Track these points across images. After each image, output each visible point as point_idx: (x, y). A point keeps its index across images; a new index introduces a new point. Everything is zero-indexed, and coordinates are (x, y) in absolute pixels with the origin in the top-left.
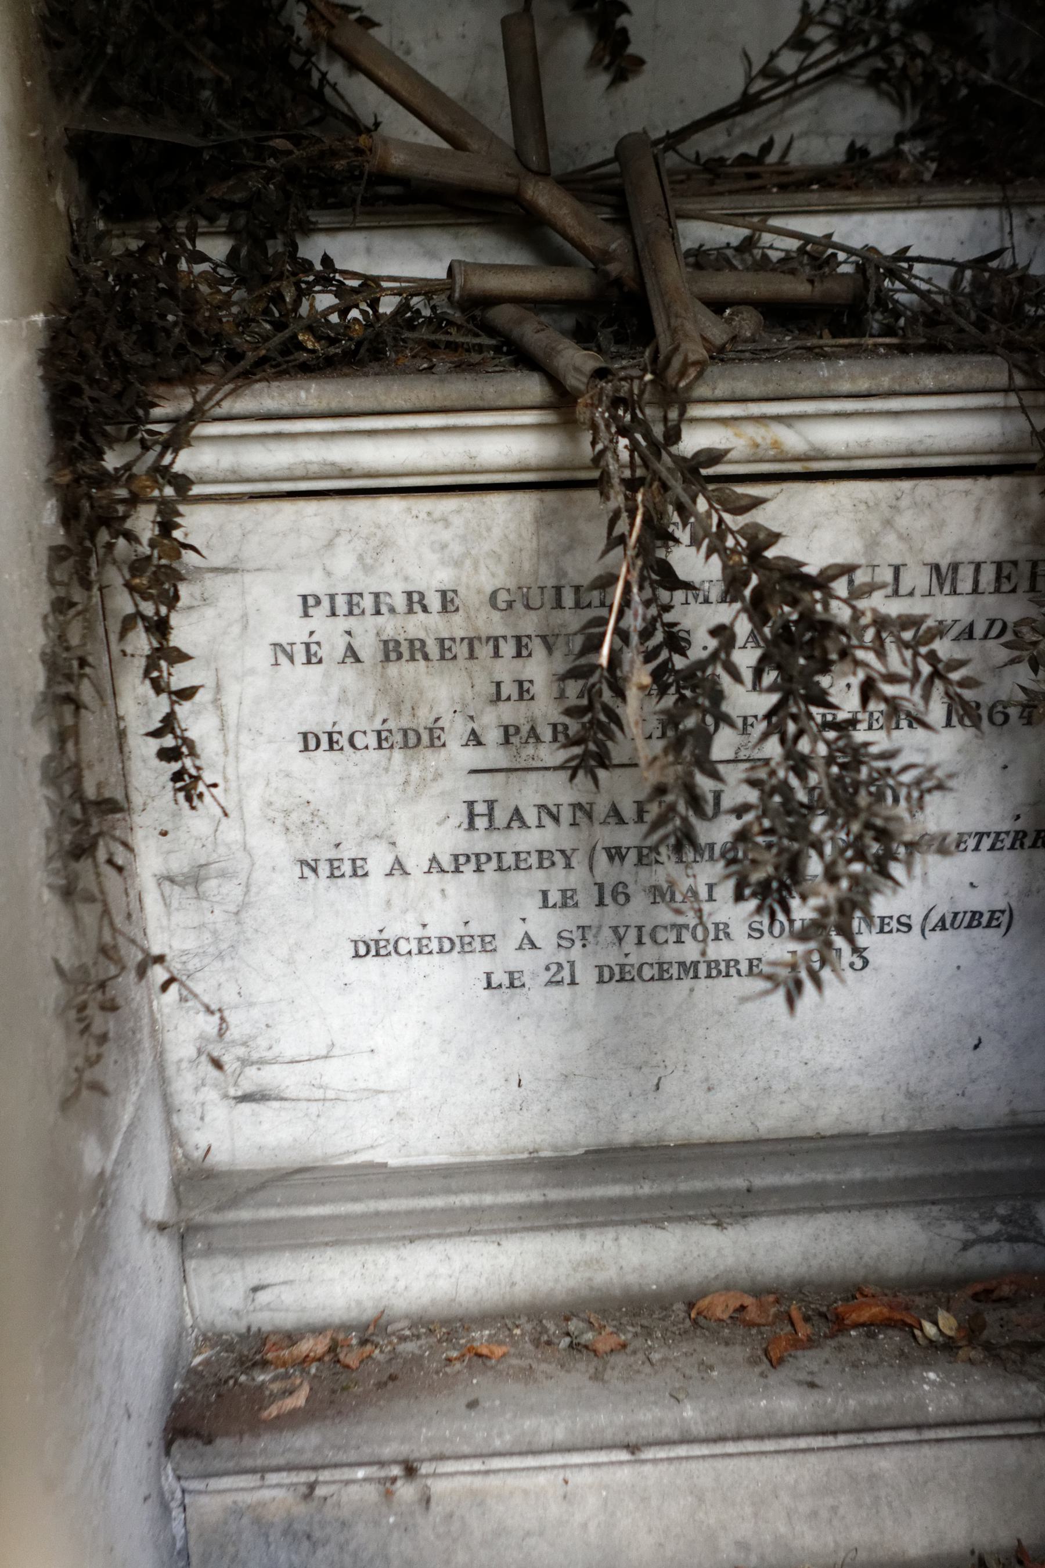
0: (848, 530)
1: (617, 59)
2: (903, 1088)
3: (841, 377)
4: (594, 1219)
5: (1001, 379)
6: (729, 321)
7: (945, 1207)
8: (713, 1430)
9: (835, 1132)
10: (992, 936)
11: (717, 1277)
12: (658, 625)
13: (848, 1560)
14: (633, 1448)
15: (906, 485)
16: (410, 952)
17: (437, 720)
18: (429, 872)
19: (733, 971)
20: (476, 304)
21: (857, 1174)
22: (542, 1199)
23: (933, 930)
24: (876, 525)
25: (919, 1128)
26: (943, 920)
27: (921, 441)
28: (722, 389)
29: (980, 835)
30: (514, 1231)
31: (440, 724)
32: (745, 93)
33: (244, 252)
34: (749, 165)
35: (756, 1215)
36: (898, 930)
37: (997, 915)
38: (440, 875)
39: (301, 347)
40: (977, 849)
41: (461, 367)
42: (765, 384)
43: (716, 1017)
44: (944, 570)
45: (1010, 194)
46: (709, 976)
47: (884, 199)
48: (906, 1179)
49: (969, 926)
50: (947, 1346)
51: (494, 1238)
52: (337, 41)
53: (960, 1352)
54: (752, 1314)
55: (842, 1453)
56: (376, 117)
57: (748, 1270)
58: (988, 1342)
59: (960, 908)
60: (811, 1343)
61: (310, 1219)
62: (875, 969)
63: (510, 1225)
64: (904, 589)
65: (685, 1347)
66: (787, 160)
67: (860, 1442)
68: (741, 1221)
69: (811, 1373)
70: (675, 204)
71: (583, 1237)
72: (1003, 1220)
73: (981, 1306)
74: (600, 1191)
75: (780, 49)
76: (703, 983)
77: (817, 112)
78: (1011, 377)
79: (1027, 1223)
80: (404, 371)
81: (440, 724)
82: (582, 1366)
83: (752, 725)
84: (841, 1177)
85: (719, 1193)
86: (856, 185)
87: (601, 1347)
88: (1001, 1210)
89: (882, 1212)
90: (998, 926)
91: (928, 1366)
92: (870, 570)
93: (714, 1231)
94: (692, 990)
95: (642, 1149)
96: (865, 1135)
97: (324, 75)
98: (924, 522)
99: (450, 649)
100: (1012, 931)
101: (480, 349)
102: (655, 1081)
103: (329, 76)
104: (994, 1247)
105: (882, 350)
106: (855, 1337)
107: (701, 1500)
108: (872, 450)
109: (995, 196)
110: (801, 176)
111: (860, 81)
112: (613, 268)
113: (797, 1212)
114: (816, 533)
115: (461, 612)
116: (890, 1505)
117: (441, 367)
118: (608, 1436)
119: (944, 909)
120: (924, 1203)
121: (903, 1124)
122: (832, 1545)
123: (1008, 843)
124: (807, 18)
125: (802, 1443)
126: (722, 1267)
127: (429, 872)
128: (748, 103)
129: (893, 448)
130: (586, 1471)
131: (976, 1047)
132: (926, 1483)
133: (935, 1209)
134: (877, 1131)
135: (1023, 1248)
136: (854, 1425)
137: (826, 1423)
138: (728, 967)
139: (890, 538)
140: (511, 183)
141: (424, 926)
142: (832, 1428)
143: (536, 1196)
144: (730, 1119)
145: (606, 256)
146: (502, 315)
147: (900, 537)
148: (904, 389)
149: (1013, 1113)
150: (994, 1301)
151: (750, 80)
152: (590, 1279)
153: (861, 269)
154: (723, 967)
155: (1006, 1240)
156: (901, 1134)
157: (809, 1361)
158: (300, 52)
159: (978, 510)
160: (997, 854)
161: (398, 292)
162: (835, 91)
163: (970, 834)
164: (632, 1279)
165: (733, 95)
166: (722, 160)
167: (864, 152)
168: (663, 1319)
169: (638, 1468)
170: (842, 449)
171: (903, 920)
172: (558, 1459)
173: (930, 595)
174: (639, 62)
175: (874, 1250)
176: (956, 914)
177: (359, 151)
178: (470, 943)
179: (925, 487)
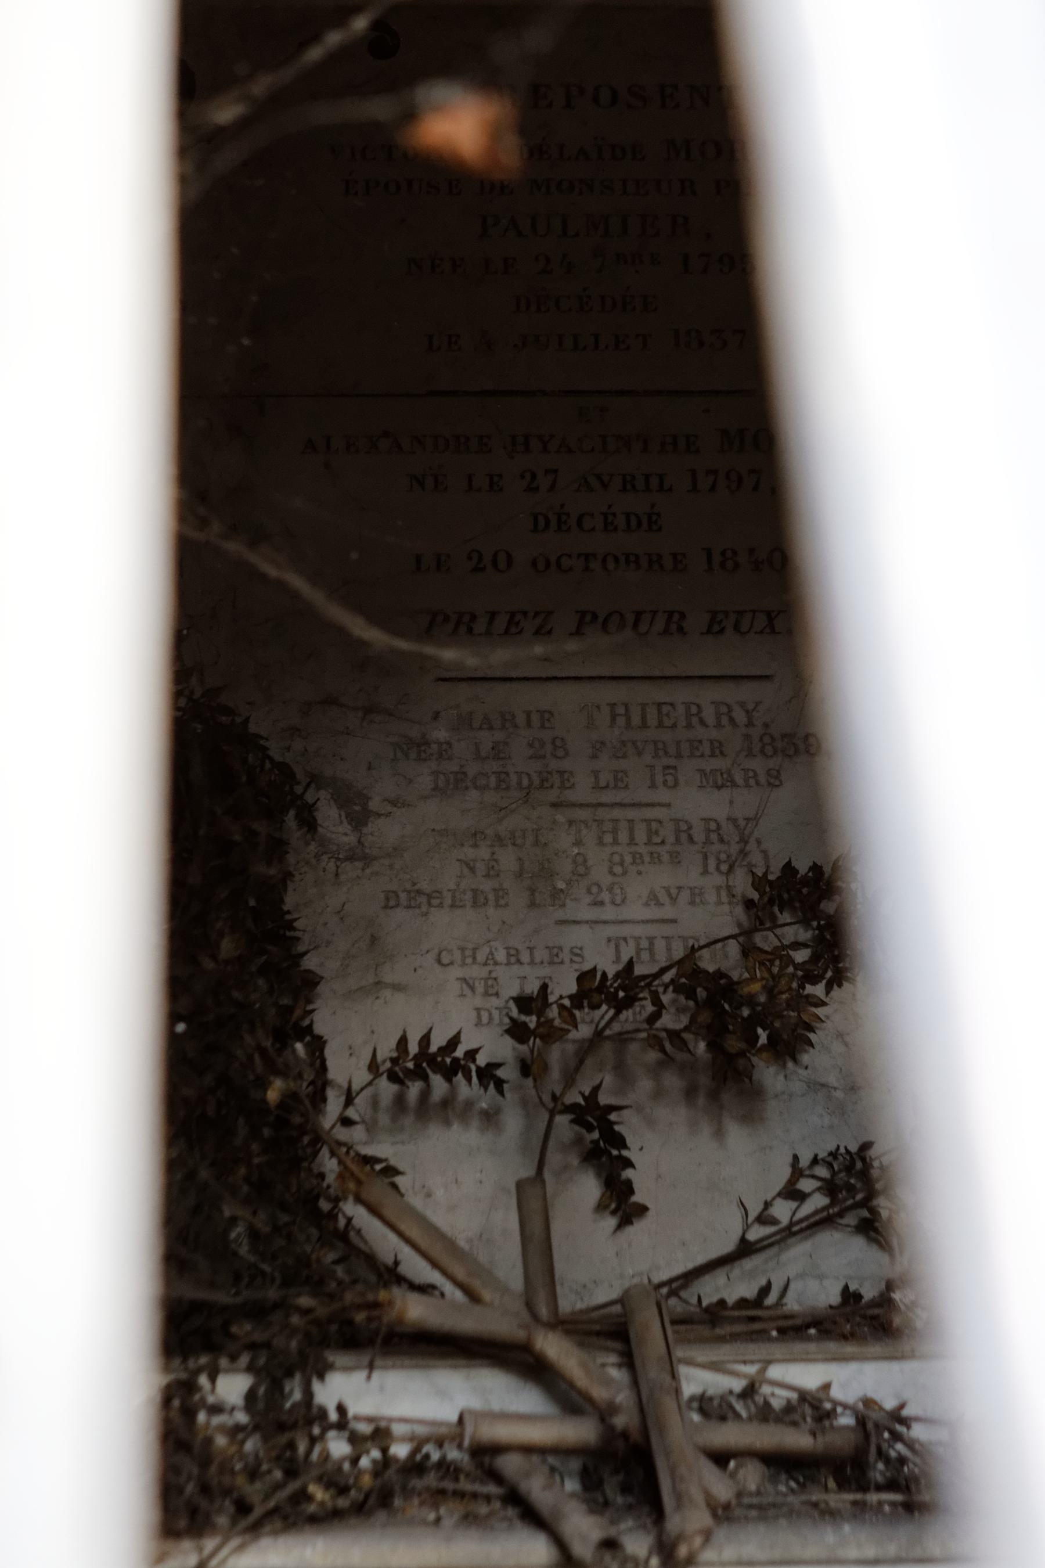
1: (622, 1204)
6: (733, 1475)
20: (486, 1454)
32: (743, 1240)
33: (262, 1391)
34: (748, 1308)
39: (310, 1498)
41: (469, 1520)
52: (364, 1195)
56: (396, 1256)
61: (342, 632)
66: (785, 1300)
70: (679, 1353)
75: (774, 1199)
80: (411, 1522)
86: (853, 1335)
97: (349, 1220)
101: (488, 1498)
103: (354, 1222)
110: (799, 1322)
111: (849, 1229)
112: (620, 1421)
117: (448, 1522)
124: (797, 1172)
128: (745, 1249)
140: (521, 1335)
145: (612, 1409)
146: (510, 1464)
151: (747, 1227)
153: (861, 1421)
158: (329, 1199)
161: (412, 1438)
165: (729, 1245)
166: (722, 1303)
167: (858, 1296)
174: (642, 1210)
177: (376, 1305)
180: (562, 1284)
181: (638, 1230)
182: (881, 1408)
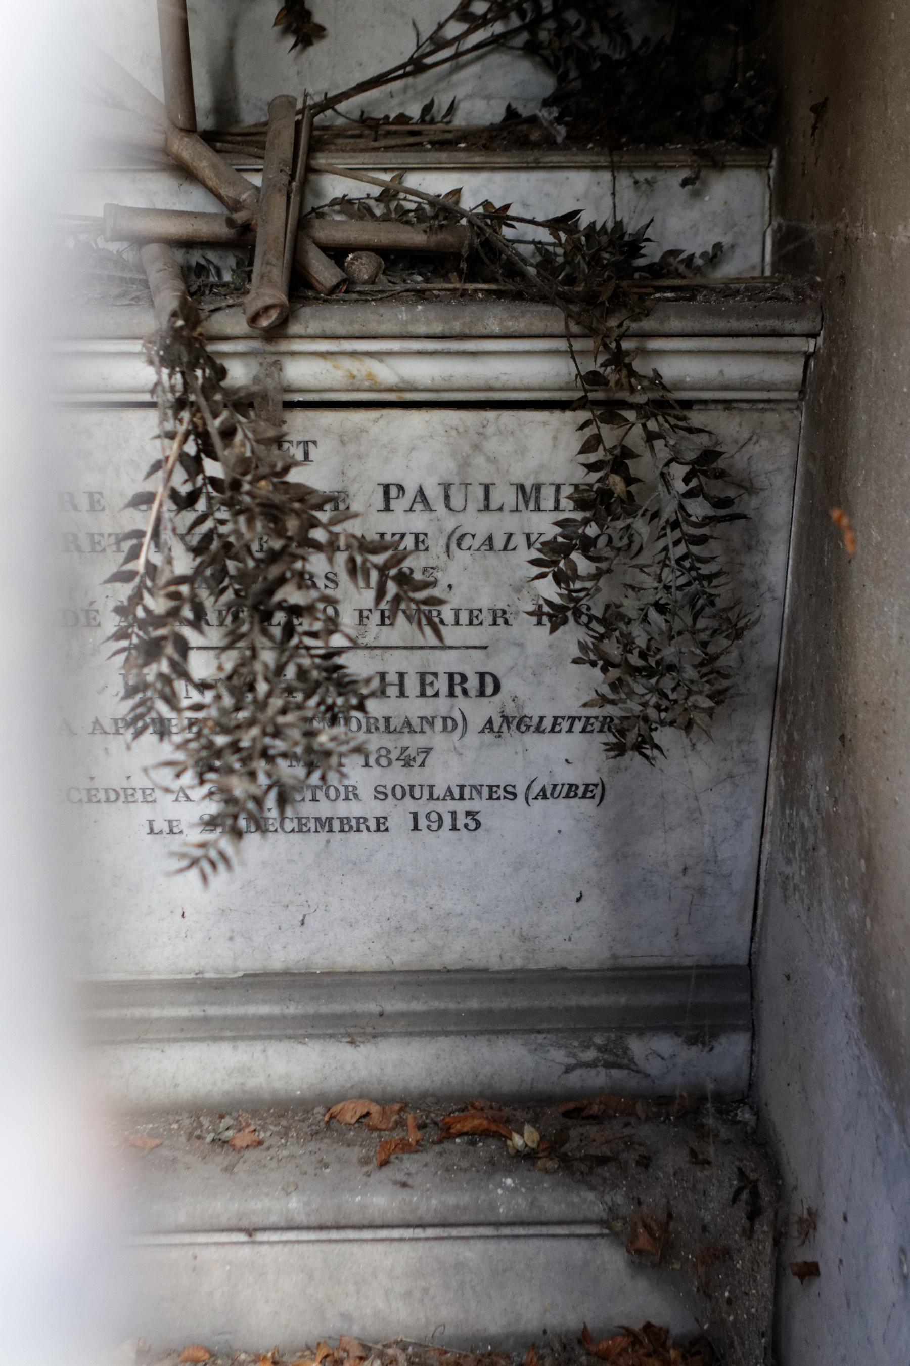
0: (442, 452)
2: (517, 932)
3: (417, 321)
4: (245, 1033)
5: (558, 327)
7: (549, 1036)
8: (314, 1220)
9: (458, 967)
10: (587, 806)
11: (352, 1087)
12: (215, 537)
13: (437, 1334)
14: (250, 1232)
15: (491, 415)
16: (80, 801)
17: (92, 603)
18: (93, 733)
19: (363, 827)
21: (474, 1004)
22: (202, 1014)
23: (536, 798)
24: (467, 449)
25: (532, 966)
26: (543, 790)
27: (497, 378)
28: (314, 327)
29: (573, 719)
30: (176, 1040)
31: (95, 607)
35: (385, 1035)
36: (505, 797)
37: (591, 788)
38: (103, 736)
40: (570, 730)
42: (351, 324)
43: (350, 865)
44: (528, 490)
45: (616, 159)
46: (342, 831)
47: (505, 160)
48: (517, 1011)
49: (567, 796)
50: (529, 1156)
51: (158, 1045)
53: (539, 1162)
54: (375, 1119)
55: (433, 1243)
57: (379, 1082)
58: (566, 1154)
59: (558, 780)
60: (418, 1147)
62: (487, 830)
63: (173, 1035)
64: (494, 505)
65: (313, 1146)
67: (446, 1235)
68: (372, 1041)
69: (409, 1174)
71: (235, 1048)
72: (599, 1049)
73: (570, 1122)
74: (252, 1010)
75: (447, 21)
76: (337, 836)
77: (480, 77)
78: (567, 326)
79: (620, 1052)
81: (95, 607)
82: (219, 1159)
83: (367, 617)
84: (461, 1006)
85: (355, 1015)
87: (238, 1143)
88: (599, 1040)
89: (494, 1038)
90: (593, 797)
91: (508, 1172)
92: (463, 486)
93: (349, 1048)
94: (328, 842)
95: (294, 975)
96: (486, 971)
98: (508, 446)
99: (99, 543)
100: (604, 802)
102: (301, 918)
104: (593, 1072)
105: (480, 295)
106: (459, 1144)
107: (311, 1277)
108: (456, 384)
109: (603, 160)
113: (420, 1034)
114: (414, 454)
115: (107, 511)
116: (473, 1288)
118: (224, 1221)
119: (544, 781)
120: (530, 1031)
121: (519, 963)
122: (423, 1321)
123: (597, 725)
125: (396, 1233)
126: (357, 1079)
127: (93, 733)
128: (416, 66)
129: (474, 383)
130: (213, 1249)
131: (578, 900)
132: (504, 1271)
133: (540, 1038)
134: (497, 968)
135: (615, 1072)
136: (436, 1221)
137: (410, 1218)
138: (358, 823)
139: (480, 461)
141: (92, 778)
142: (416, 1222)
143: (196, 1012)
144: (368, 952)
147: (488, 459)
148: (474, 333)
149: (614, 957)
150: (583, 1118)
152: (242, 1084)
154: (354, 823)
155: (604, 1066)
156: (516, 971)
157: (410, 1164)
159: (555, 438)
160: (588, 735)
162: (496, 59)
163: (563, 718)
164: (279, 1085)
168: (303, 1120)
169: (257, 1248)
170: (428, 383)
171: (509, 789)
172: (187, 1238)
173: (517, 511)
175: (488, 1070)
176: (555, 786)
178: (133, 795)
179: (507, 417)
180: (247, 102)
181: (317, 50)
182: (494, 208)
